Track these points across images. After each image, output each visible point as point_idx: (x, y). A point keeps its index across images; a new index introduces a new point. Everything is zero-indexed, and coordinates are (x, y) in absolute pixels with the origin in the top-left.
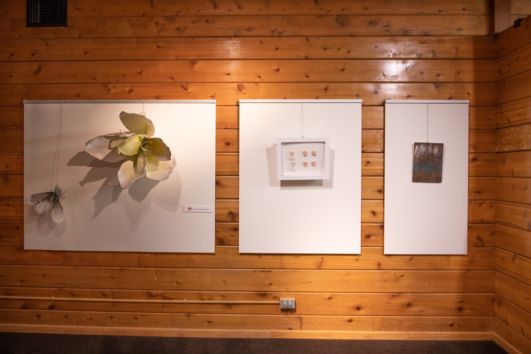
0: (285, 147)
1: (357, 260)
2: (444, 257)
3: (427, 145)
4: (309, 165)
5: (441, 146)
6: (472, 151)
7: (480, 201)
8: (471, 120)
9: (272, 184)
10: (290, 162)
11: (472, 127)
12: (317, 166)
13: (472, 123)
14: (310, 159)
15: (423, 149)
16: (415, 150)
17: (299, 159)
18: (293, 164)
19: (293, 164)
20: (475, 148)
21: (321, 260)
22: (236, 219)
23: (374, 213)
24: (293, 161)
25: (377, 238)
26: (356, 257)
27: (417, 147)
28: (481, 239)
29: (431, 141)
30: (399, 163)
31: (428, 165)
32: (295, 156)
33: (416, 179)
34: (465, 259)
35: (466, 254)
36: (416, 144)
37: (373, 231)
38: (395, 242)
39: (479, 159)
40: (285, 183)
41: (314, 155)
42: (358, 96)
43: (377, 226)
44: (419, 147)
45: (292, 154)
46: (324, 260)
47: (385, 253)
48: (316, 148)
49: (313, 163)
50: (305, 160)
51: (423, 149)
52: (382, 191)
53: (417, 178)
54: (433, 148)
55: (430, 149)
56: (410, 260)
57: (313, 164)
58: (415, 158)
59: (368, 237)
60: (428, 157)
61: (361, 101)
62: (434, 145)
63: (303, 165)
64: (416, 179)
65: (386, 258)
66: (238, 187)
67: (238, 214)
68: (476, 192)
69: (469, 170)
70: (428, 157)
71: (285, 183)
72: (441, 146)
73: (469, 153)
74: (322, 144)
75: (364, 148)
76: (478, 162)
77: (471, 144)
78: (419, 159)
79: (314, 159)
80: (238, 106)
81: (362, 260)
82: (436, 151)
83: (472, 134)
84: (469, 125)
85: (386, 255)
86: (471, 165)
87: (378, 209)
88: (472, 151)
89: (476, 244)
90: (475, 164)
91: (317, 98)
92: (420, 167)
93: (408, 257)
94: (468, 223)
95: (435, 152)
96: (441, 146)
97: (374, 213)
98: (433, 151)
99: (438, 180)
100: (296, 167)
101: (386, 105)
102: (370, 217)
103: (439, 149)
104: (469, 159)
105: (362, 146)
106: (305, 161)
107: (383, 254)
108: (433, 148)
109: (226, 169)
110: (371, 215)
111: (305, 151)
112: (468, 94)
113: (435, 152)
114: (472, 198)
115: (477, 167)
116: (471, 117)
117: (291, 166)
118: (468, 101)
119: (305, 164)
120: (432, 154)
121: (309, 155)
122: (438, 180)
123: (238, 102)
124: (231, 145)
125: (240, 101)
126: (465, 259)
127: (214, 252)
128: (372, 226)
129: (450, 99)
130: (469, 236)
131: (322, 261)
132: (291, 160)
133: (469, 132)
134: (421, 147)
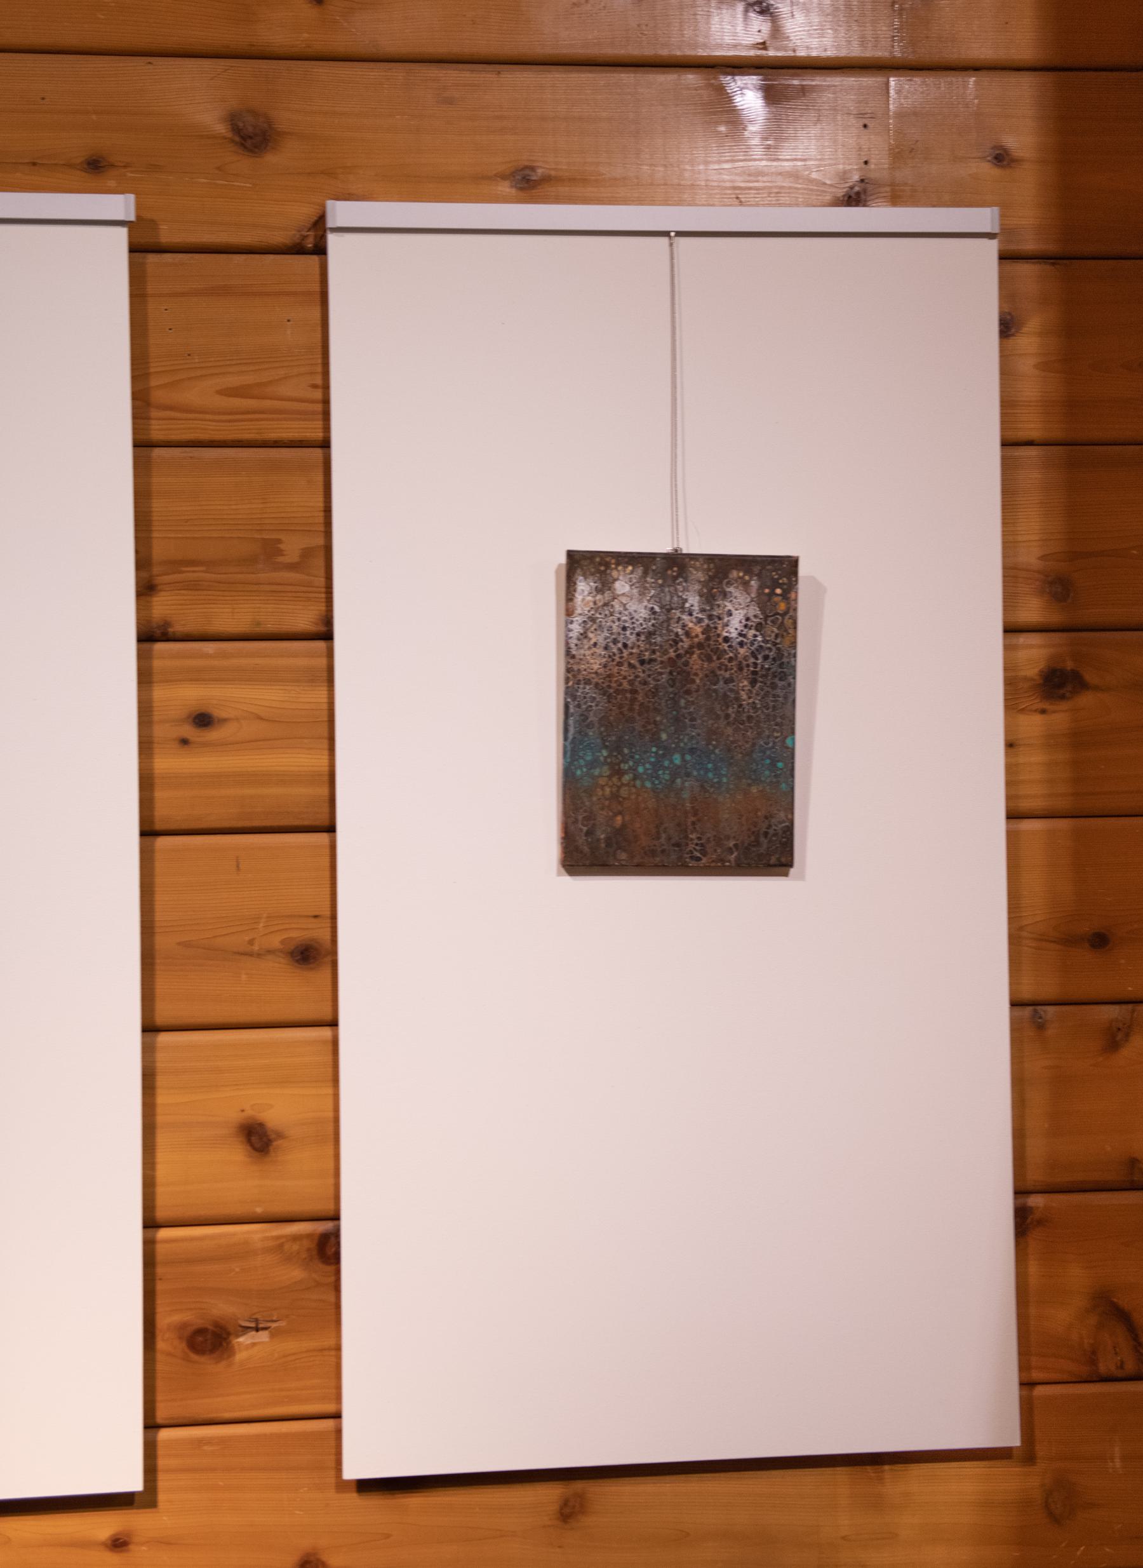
1: (118, 1544)
2: (841, 1473)
3: (674, 565)
6: (1033, 611)
7: (1112, 1012)
8: (1027, 365)
11: (1032, 427)
13: (1030, 390)
15: (632, 601)
16: (569, 612)
23: (257, 1138)
25: (290, 1345)
26: (104, 1525)
27: (584, 587)
28: (1123, 1316)
29: (697, 544)
31: (678, 745)
34: (1008, 1481)
35: (1012, 1438)
36: (579, 563)
39: (1089, 676)
42: (95, 170)
43: (295, 1238)
44: (605, 585)
47: (352, 1471)
51: (632, 601)
53: (594, 844)
54: (712, 595)
55: (693, 601)
56: (568, 1513)
58: (574, 678)
60: (679, 669)
62: (722, 569)
68: (1069, 941)
69: (1011, 771)
70: (679, 669)
73: (1009, 630)
75: (163, 606)
76: (1086, 700)
77: (1031, 556)
78: (606, 686)
80: (320, 250)
81: (165, 1542)
82: (738, 614)
83: (1031, 477)
84: (1008, 405)
85: (366, 1486)
86: (1033, 725)
87: (279, 1109)
88: (1033, 611)
89: (1092, 1357)
90: (1060, 717)
92: (617, 748)
93: (551, 1493)
94: (1019, 1192)
95: (734, 626)
97: (257, 1138)
99: (764, 847)
103: (764, 602)
107: (343, 1486)
108: (712, 595)
110: (237, 1154)
112: (1001, 158)
113: (734, 626)
114: (1049, 988)
115: (1079, 742)
116: (1028, 342)
120: (710, 644)
122: (764, 847)
123: (320, 225)
125: (341, 212)
126: (1008, 1481)
127: (134, 1482)
129: (854, 199)
130: (1025, 1297)
133: (1007, 465)
134: (622, 586)
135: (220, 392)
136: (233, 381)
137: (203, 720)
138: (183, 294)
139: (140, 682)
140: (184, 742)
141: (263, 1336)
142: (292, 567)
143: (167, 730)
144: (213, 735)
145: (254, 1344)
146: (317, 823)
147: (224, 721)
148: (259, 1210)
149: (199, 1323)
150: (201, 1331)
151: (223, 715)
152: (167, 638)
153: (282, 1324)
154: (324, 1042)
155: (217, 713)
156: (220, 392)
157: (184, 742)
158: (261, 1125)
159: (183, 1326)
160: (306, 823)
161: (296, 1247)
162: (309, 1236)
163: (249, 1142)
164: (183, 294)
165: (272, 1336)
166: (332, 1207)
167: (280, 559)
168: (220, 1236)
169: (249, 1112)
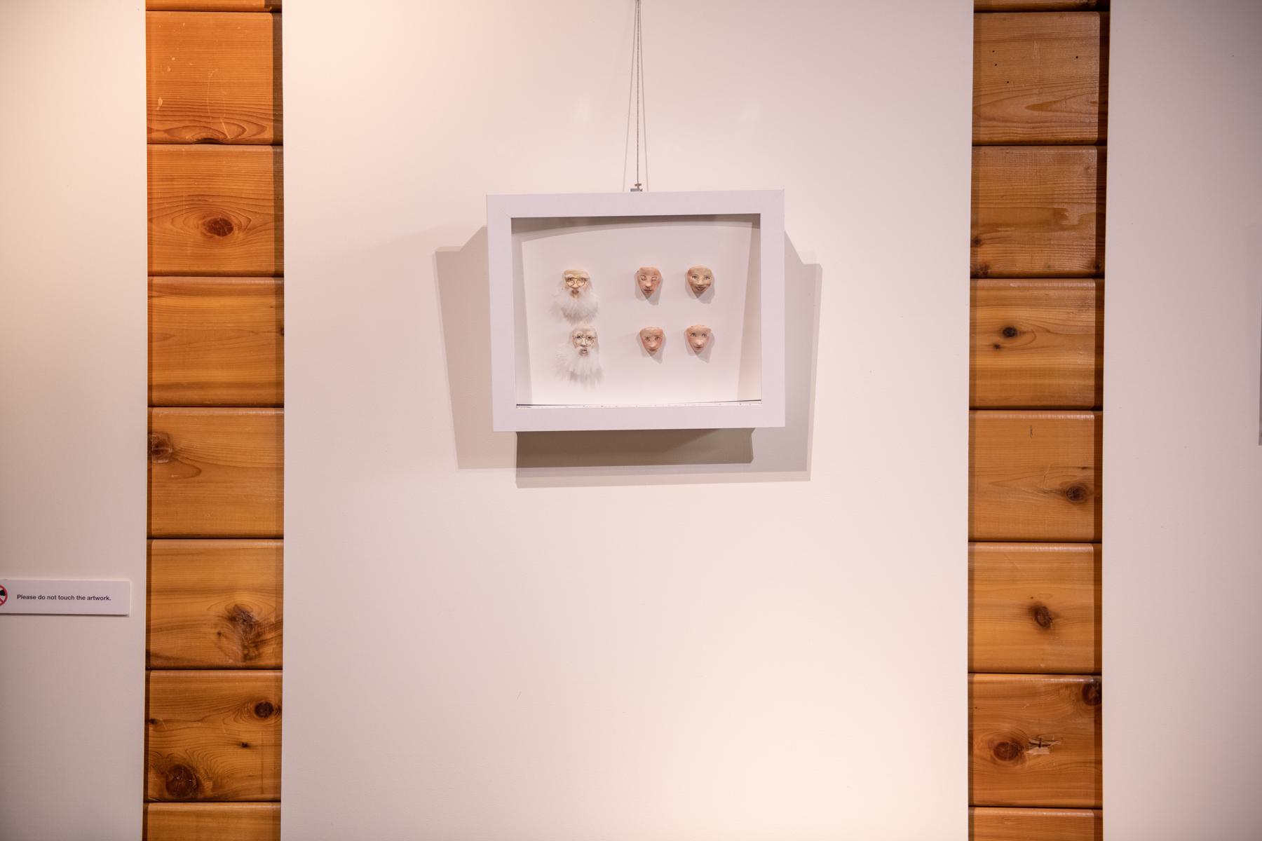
0: (534, 246)
4: (674, 345)
9: (469, 452)
10: (567, 327)
12: (715, 350)
14: (675, 313)
18: (584, 343)
19: (584, 343)
22: (268, 650)
23: (1041, 617)
24: (582, 325)
25: (1062, 758)
32: (593, 297)
40: (543, 451)
41: (699, 290)
43: (1067, 686)
48: (713, 249)
50: (648, 316)
52: (1086, 493)
57: (698, 341)
59: (1010, 750)
63: (638, 347)
66: (280, 469)
67: (278, 625)
71: (543, 451)
74: (746, 230)
75: (988, 253)
79: (696, 314)
87: (1064, 597)
97: (1041, 617)
100: (598, 358)
105: (976, 242)
106: (652, 325)
110: (1027, 627)
111: (648, 265)
117: (571, 352)
119: (651, 342)
124: (237, 235)
128: (1032, 692)
132: (573, 317)
135: (1028, 107)
136: (1035, 100)
137: (1010, 332)
138: (1004, 41)
139: (972, 306)
140: (997, 347)
141: (1044, 751)
142: (1073, 228)
143: (996, 336)
144: (1019, 341)
145: (1039, 756)
146: (1086, 404)
147: (1024, 333)
148: (1043, 665)
149: (998, 741)
150: (1003, 745)
151: (1024, 328)
152: (986, 276)
153: (1059, 743)
154: (1089, 553)
155: (1021, 327)
156: (1028, 107)
157: (997, 347)
158: (1045, 608)
159: (991, 741)
160: (1079, 404)
161: (1067, 692)
162: (1078, 685)
163: (1036, 619)
164: (1004, 41)
165: (1051, 751)
166: (268, 782)
167: (1065, 223)
168: (1011, 682)
169: (1037, 599)
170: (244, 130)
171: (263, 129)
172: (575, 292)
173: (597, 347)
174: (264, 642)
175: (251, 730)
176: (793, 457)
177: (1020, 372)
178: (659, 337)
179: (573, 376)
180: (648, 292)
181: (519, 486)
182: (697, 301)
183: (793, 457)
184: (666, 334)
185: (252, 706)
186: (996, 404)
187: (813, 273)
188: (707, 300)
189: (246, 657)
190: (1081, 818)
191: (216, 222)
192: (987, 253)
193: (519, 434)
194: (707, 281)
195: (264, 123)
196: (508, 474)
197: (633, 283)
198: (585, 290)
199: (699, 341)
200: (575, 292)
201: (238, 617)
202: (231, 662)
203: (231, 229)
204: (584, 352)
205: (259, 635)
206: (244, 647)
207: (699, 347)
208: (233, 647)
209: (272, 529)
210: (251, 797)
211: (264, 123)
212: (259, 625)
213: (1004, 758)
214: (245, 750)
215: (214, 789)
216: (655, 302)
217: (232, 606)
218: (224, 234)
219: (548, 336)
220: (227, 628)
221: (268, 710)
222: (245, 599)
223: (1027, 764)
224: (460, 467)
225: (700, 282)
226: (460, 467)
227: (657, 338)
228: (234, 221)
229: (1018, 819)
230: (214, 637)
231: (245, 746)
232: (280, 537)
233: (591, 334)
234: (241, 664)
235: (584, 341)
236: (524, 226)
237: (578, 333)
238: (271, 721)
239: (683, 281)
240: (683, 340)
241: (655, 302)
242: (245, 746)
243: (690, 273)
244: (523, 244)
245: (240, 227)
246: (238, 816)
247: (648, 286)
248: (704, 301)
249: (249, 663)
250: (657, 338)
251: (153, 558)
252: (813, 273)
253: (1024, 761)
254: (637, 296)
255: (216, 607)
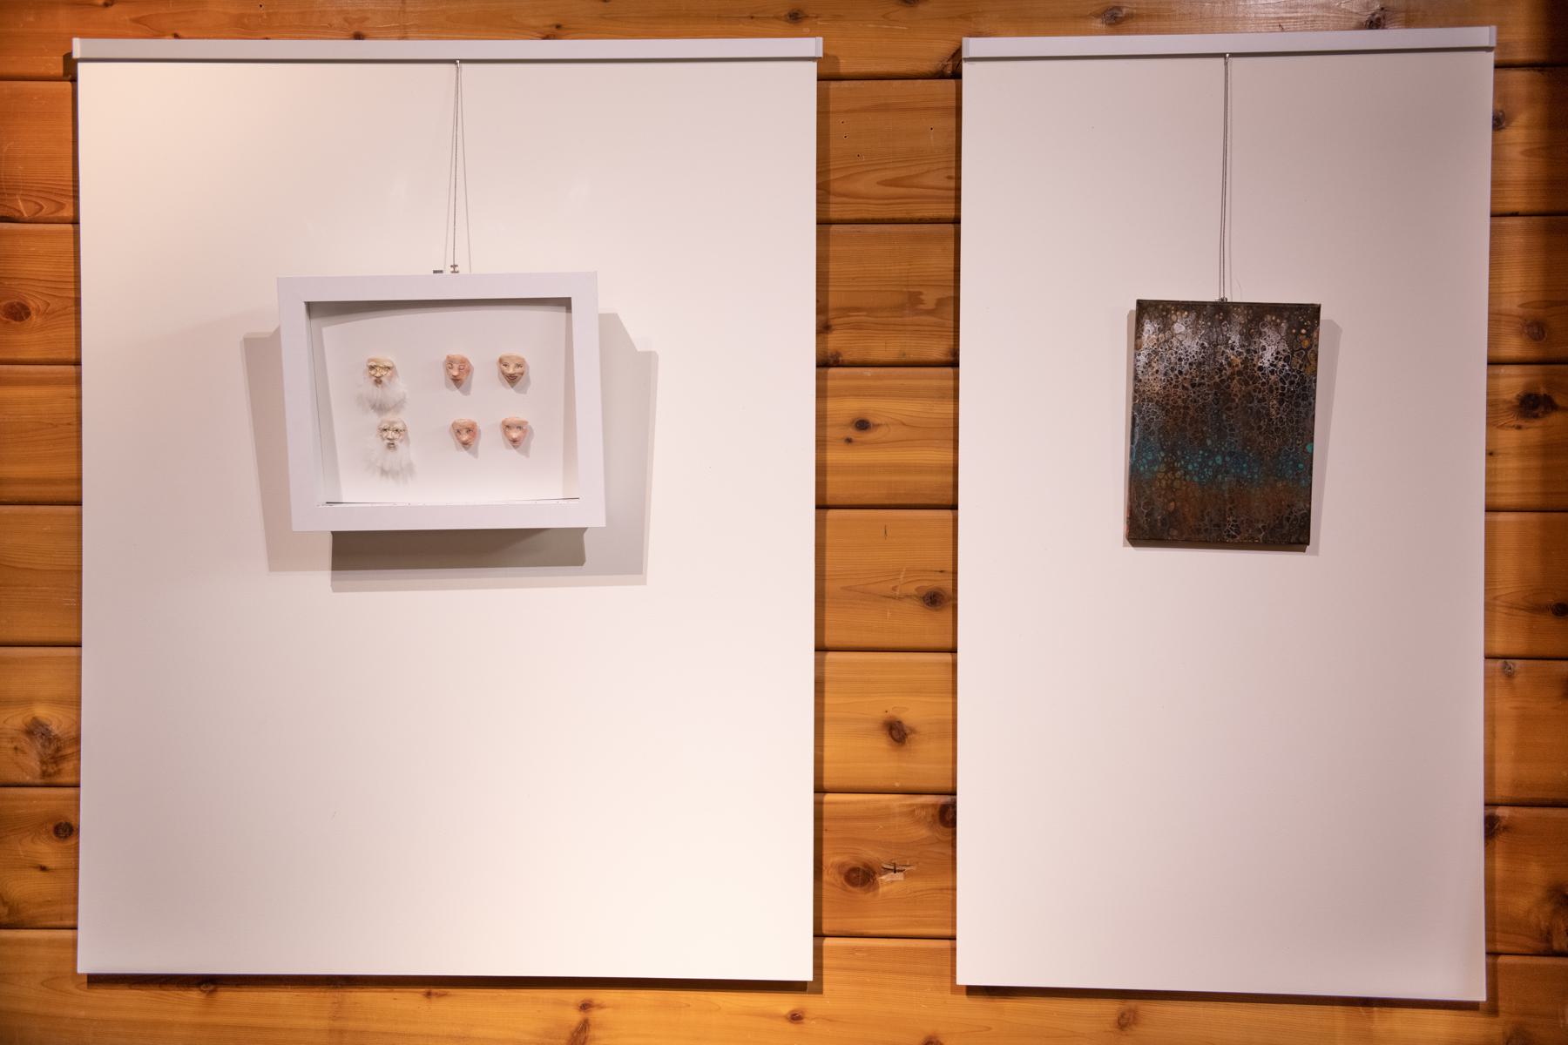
0: (334, 332)
1: (795, 1017)
3: (1220, 311)
4: (490, 438)
5: (1302, 321)
9: (282, 550)
10: (375, 419)
11: (1517, 201)
12: (535, 444)
14: (489, 404)
15: (1187, 338)
16: (1138, 347)
17: (427, 406)
18: (392, 437)
19: (392, 437)
20: (1536, 329)
21: (575, 1017)
22: (67, 766)
23: (897, 732)
24: (390, 417)
25: (919, 884)
26: (785, 1003)
27: (1149, 327)
29: (1235, 297)
30: (1043, 425)
31: (1223, 445)
32: (399, 387)
33: (1147, 528)
35: (1478, 993)
37: (886, 840)
38: (1015, 916)
39: (1558, 400)
40: (360, 552)
41: (512, 379)
43: (923, 806)
44: (1166, 326)
45: (378, 373)
46: (596, 1015)
48: (522, 335)
49: (507, 427)
50: (461, 407)
51: (1187, 338)
52: (941, 599)
55: (1235, 338)
57: (516, 435)
58: (1140, 398)
59: (862, 877)
61: (812, 46)
62: (1258, 314)
63: (450, 440)
64: (1147, 528)
65: (982, 1009)
66: (79, 572)
67: (77, 740)
71: (360, 552)
72: (1303, 319)
74: (558, 315)
75: (835, 341)
76: (1555, 419)
79: (512, 405)
80: (957, 75)
81: (829, 1020)
85: (972, 990)
86: (1510, 438)
87: (912, 712)
88: (1513, 347)
89: (1547, 936)
90: (1533, 432)
91: (555, 32)
93: (1112, 1007)
95: (1267, 358)
96: (1302, 321)
97: (897, 732)
98: (1251, 352)
99: (1288, 529)
100: (407, 452)
101: (966, 66)
102: (871, 758)
103: (1292, 340)
104: (1492, 405)
105: (823, 329)
106: (465, 417)
107: (956, 989)
109: (893, 405)
110: (882, 743)
111: (456, 352)
113: (1267, 358)
114: (1518, 645)
115: (1549, 451)
117: (376, 444)
118: (1484, 35)
119: (466, 435)
120: (1248, 372)
121: (484, 376)
122: (1288, 529)
123: (957, 56)
124: (35, 319)
125: (78, 47)
126: (1474, 1026)
128: (884, 814)
129: (1374, 24)
131: (585, 1026)
132: (380, 408)
134: (1179, 328)
136: (889, 175)
137: (862, 425)
140: (849, 441)
141: (899, 876)
142: (929, 312)
149: (854, 863)
150: (854, 870)
151: (878, 421)
157: (849, 441)
159: (842, 865)
162: (933, 805)
168: (864, 802)
169: (891, 713)
170: (42, 208)
171: (61, 206)
172: (378, 381)
173: (407, 439)
174: (64, 758)
175: (47, 850)
176: (629, 562)
177: (869, 468)
178: (471, 430)
179: (384, 472)
180: (456, 381)
181: (335, 590)
182: (512, 391)
183: (629, 562)
184: (481, 426)
185: (51, 826)
186: (848, 502)
187: (648, 361)
188: (523, 390)
189: (44, 774)
190: (889, 949)
191: (12, 306)
192: (835, 341)
193: (334, 533)
194: (519, 370)
195: (63, 200)
196: (322, 577)
197: (442, 371)
198: (390, 378)
199: (515, 434)
200: (378, 381)
201: (35, 730)
202: (28, 779)
203: (28, 314)
204: (391, 445)
205: (58, 749)
206: (43, 763)
207: (514, 441)
208: (32, 763)
209: (72, 637)
210: (49, 924)
211: (63, 200)
212: (57, 738)
213: (854, 884)
214: (42, 874)
215: (9, 914)
216: (466, 392)
217: (29, 719)
218: (21, 319)
219: (354, 428)
220: (24, 742)
221: (66, 830)
222: (41, 712)
223: (882, 889)
224: (272, 568)
225: (511, 371)
226: (272, 568)
227: (469, 430)
228: (32, 304)
229: (870, 950)
230: (11, 752)
231: (43, 869)
232: (78, 645)
233: (399, 426)
234: (39, 781)
235: (391, 434)
236: (315, 309)
237: (385, 425)
238: (71, 842)
239: (495, 370)
240: (499, 433)
241: (466, 392)
242: (43, 869)
243: (501, 361)
244: (325, 330)
245: (38, 311)
246: (35, 943)
247: (458, 375)
248: (519, 391)
249: (47, 780)
250: (469, 430)
251: (827, 729)
252: (648, 361)
253: (877, 888)
254: (448, 386)
255: (15, 720)
